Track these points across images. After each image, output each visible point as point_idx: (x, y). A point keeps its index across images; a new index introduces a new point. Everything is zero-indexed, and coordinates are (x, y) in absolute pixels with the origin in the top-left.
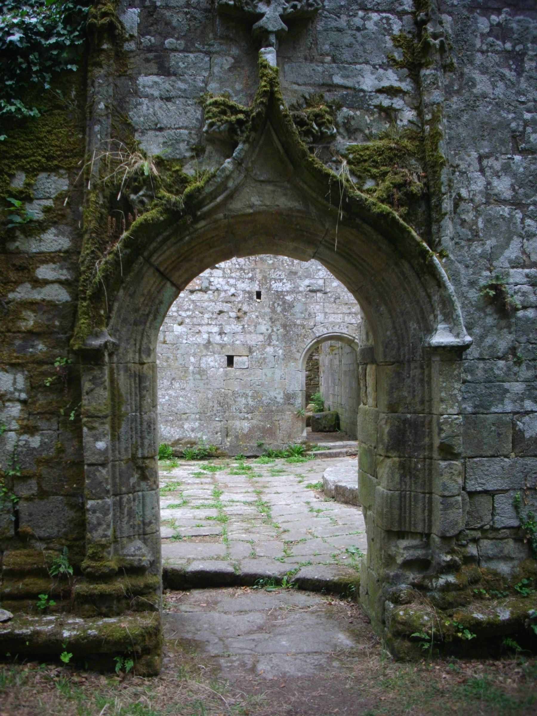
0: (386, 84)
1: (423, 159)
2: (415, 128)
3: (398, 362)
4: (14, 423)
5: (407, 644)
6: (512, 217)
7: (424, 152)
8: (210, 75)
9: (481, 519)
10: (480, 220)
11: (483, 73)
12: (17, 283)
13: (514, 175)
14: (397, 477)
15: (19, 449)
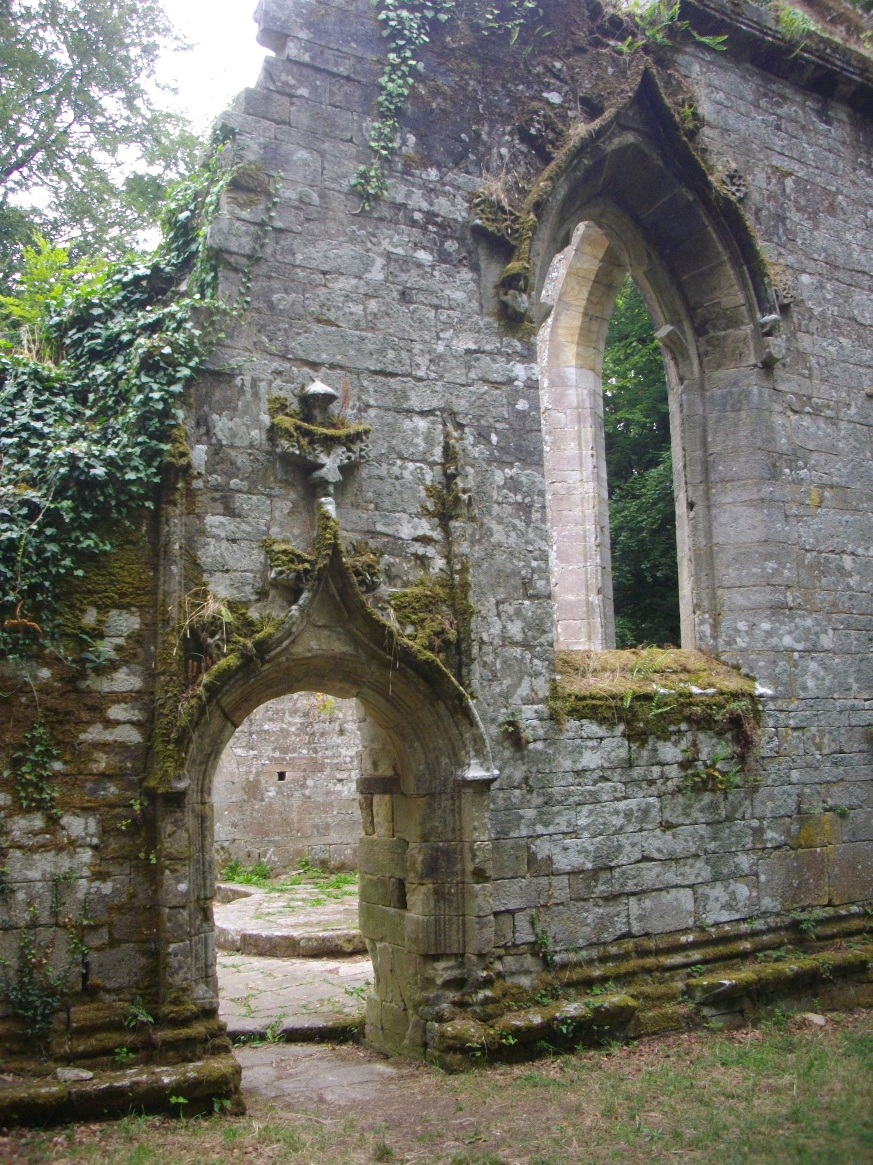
0: (420, 532)
1: (452, 605)
2: (444, 576)
3: (429, 794)
4: (85, 869)
5: (459, 1056)
6: (523, 657)
7: (453, 599)
8: (272, 519)
9: (504, 936)
10: (498, 661)
11: (499, 523)
12: (89, 723)
13: (524, 619)
14: (432, 902)
15: (91, 897)
